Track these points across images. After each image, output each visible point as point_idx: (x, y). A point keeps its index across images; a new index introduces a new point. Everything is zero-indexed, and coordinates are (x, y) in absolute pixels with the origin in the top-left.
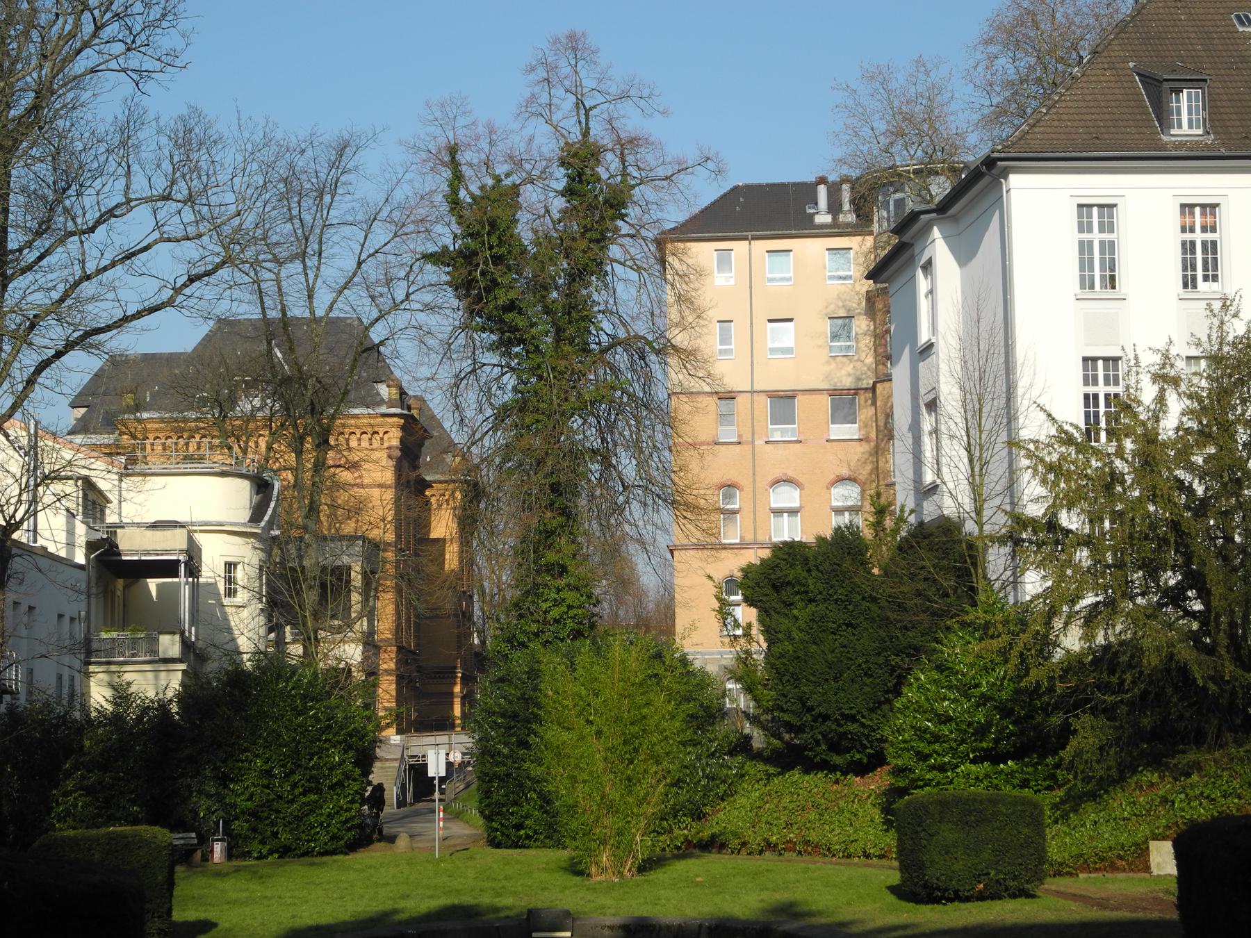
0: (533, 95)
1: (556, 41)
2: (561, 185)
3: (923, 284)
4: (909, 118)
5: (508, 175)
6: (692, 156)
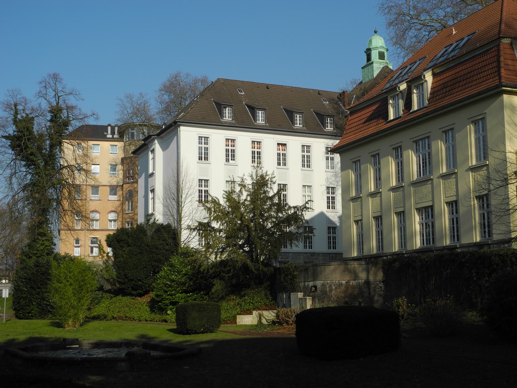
0: (40, 91)
1: (50, 75)
2: (49, 118)
3: (151, 156)
4: (138, 110)
5: (30, 114)
6: (89, 113)
